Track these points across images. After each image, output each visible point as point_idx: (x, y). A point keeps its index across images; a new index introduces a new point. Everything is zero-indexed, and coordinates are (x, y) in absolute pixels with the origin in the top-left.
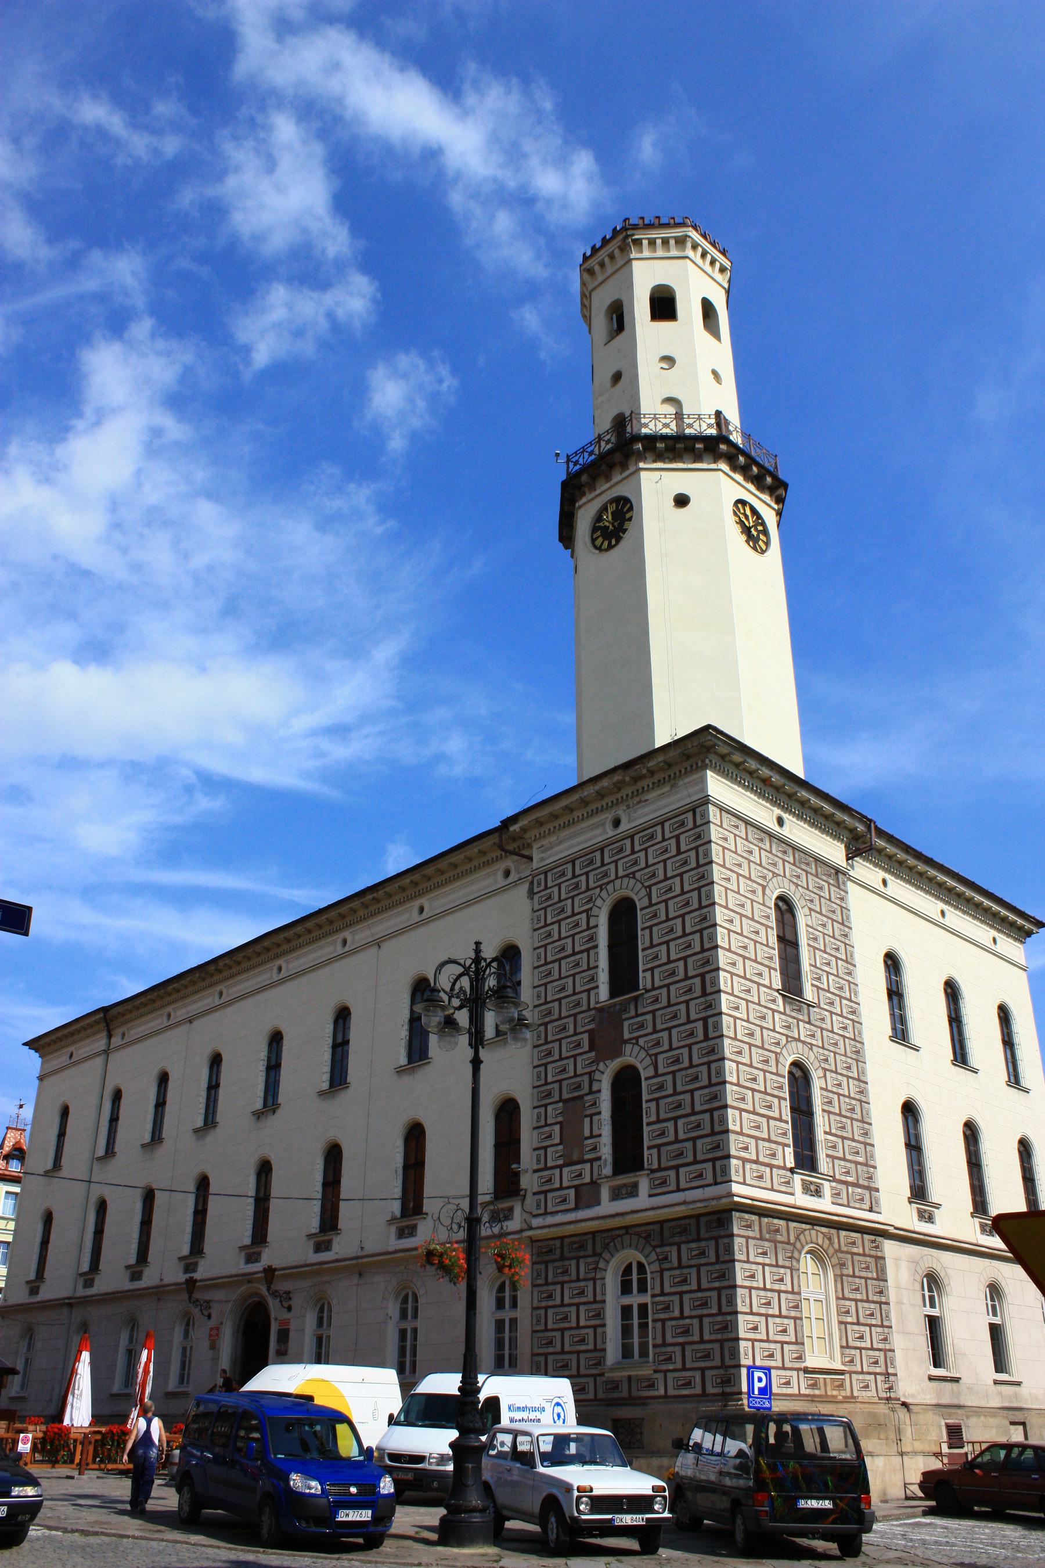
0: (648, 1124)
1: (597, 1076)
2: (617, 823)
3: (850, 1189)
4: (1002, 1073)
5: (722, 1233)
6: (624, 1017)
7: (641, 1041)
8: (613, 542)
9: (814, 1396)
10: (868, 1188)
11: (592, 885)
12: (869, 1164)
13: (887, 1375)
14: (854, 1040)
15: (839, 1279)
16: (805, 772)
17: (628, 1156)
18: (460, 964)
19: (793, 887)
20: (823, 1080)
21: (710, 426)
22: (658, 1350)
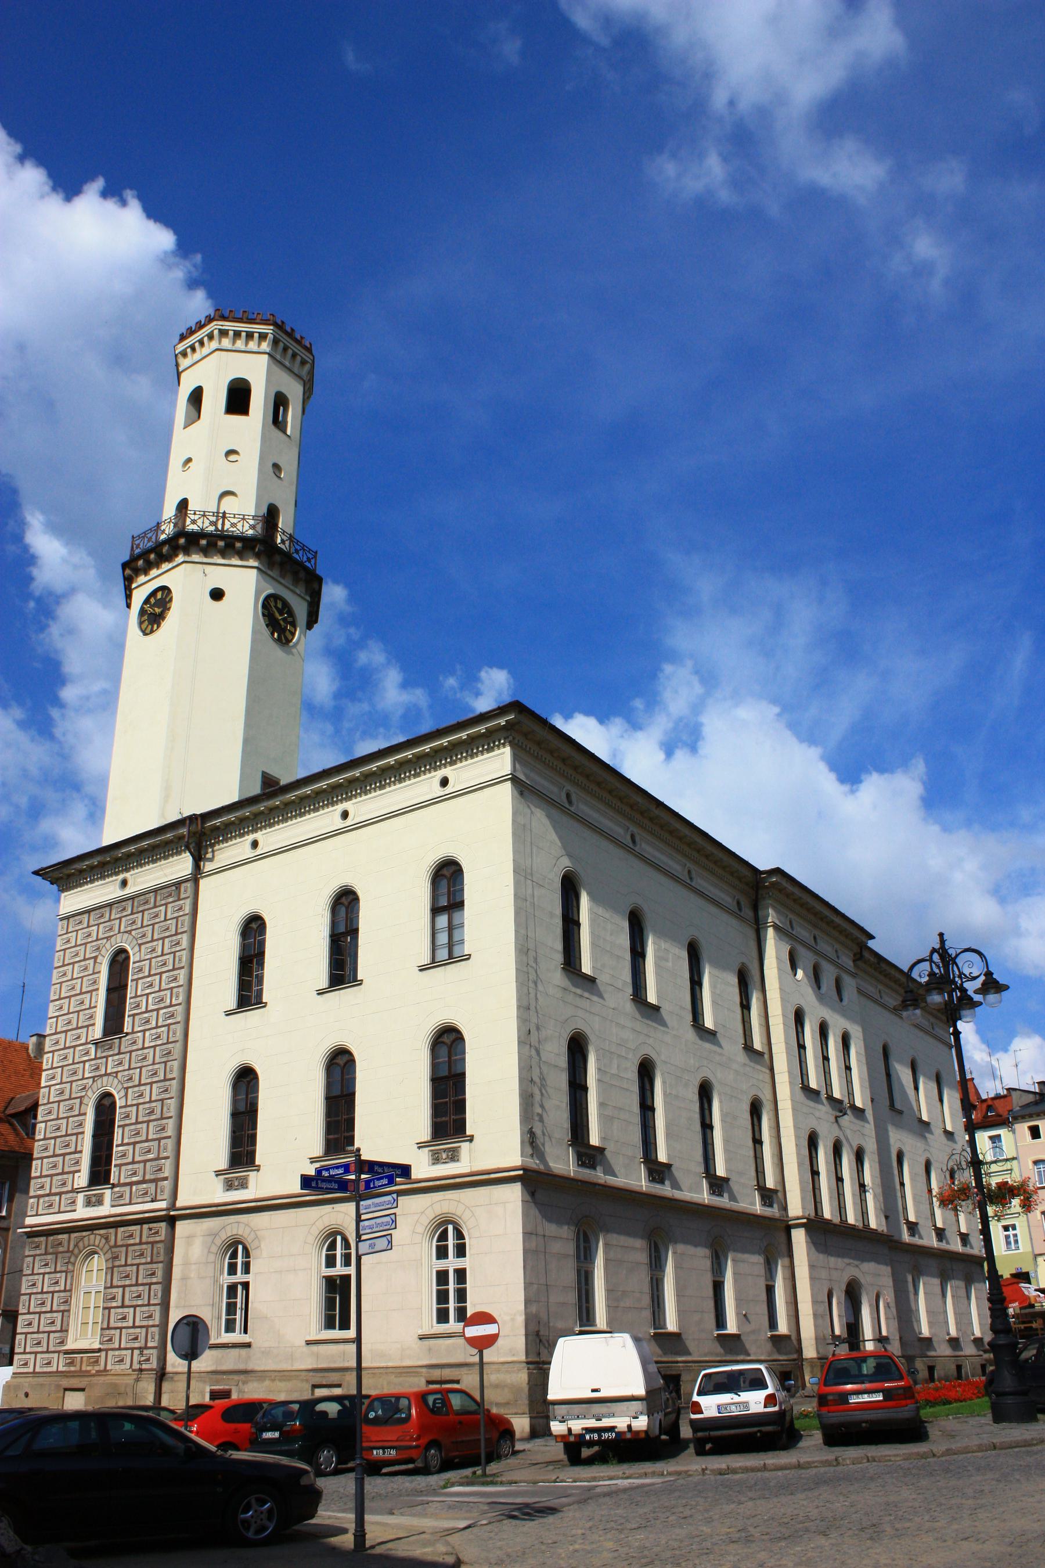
1: (85, 1101)
8: (155, 627)
9: (69, 1372)
17: (100, 1175)
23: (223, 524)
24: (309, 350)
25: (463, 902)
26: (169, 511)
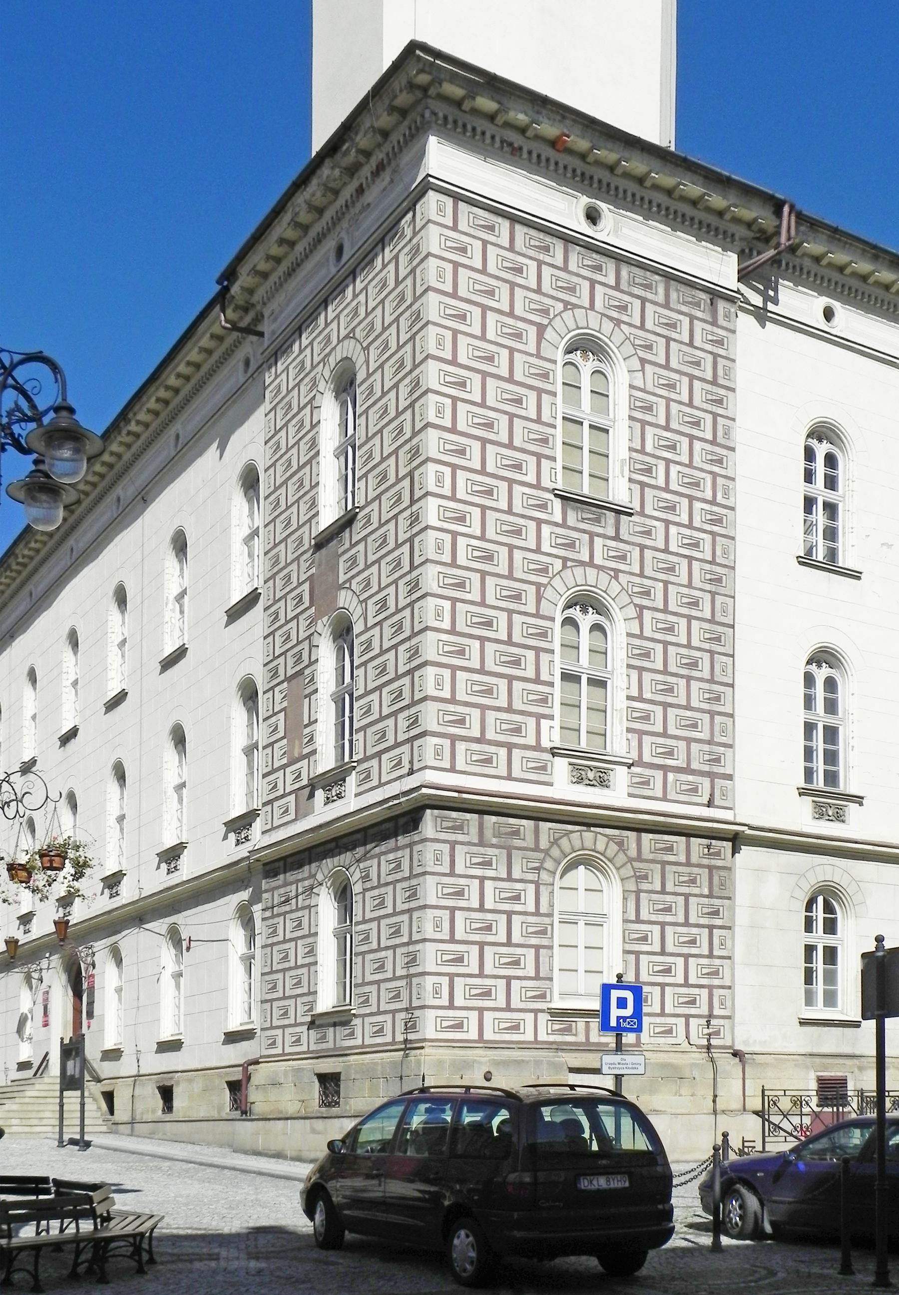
1: (549, 334)
5: (416, 838)
12: (719, 747)
15: (632, 897)
19: (608, 326)
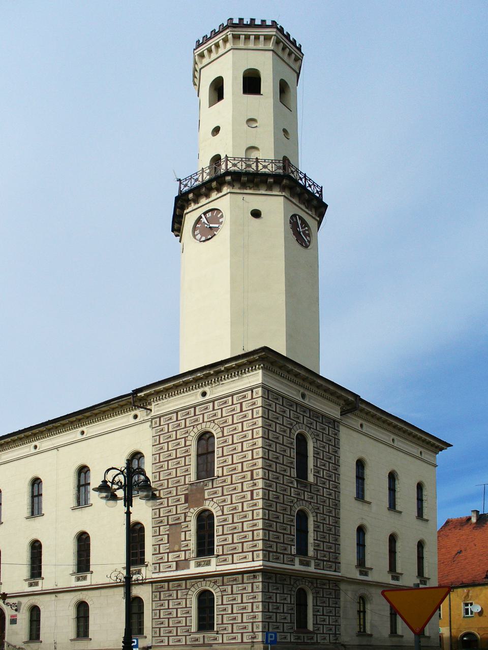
0: (217, 536)
2: (204, 394)
3: (325, 563)
4: (368, 473)
6: (205, 488)
7: (215, 500)
10: (335, 563)
11: (188, 425)
13: (335, 634)
14: (335, 499)
15: (315, 598)
16: (289, 336)
17: (205, 547)
18: (118, 470)
20: (316, 517)
21: (279, 168)
22: (219, 626)
23: (257, 166)
24: (299, 49)
25: (89, 483)
26: (205, 162)
